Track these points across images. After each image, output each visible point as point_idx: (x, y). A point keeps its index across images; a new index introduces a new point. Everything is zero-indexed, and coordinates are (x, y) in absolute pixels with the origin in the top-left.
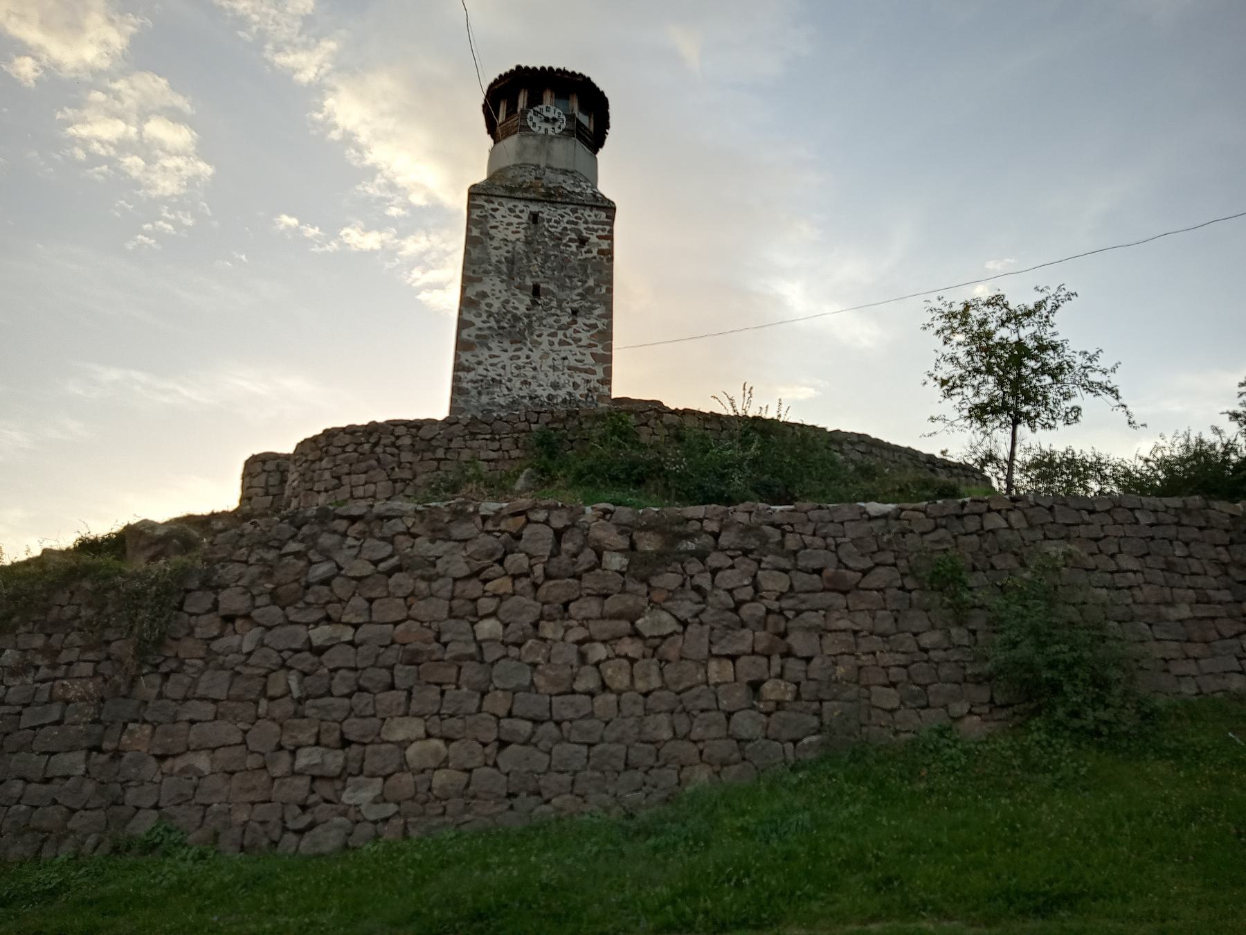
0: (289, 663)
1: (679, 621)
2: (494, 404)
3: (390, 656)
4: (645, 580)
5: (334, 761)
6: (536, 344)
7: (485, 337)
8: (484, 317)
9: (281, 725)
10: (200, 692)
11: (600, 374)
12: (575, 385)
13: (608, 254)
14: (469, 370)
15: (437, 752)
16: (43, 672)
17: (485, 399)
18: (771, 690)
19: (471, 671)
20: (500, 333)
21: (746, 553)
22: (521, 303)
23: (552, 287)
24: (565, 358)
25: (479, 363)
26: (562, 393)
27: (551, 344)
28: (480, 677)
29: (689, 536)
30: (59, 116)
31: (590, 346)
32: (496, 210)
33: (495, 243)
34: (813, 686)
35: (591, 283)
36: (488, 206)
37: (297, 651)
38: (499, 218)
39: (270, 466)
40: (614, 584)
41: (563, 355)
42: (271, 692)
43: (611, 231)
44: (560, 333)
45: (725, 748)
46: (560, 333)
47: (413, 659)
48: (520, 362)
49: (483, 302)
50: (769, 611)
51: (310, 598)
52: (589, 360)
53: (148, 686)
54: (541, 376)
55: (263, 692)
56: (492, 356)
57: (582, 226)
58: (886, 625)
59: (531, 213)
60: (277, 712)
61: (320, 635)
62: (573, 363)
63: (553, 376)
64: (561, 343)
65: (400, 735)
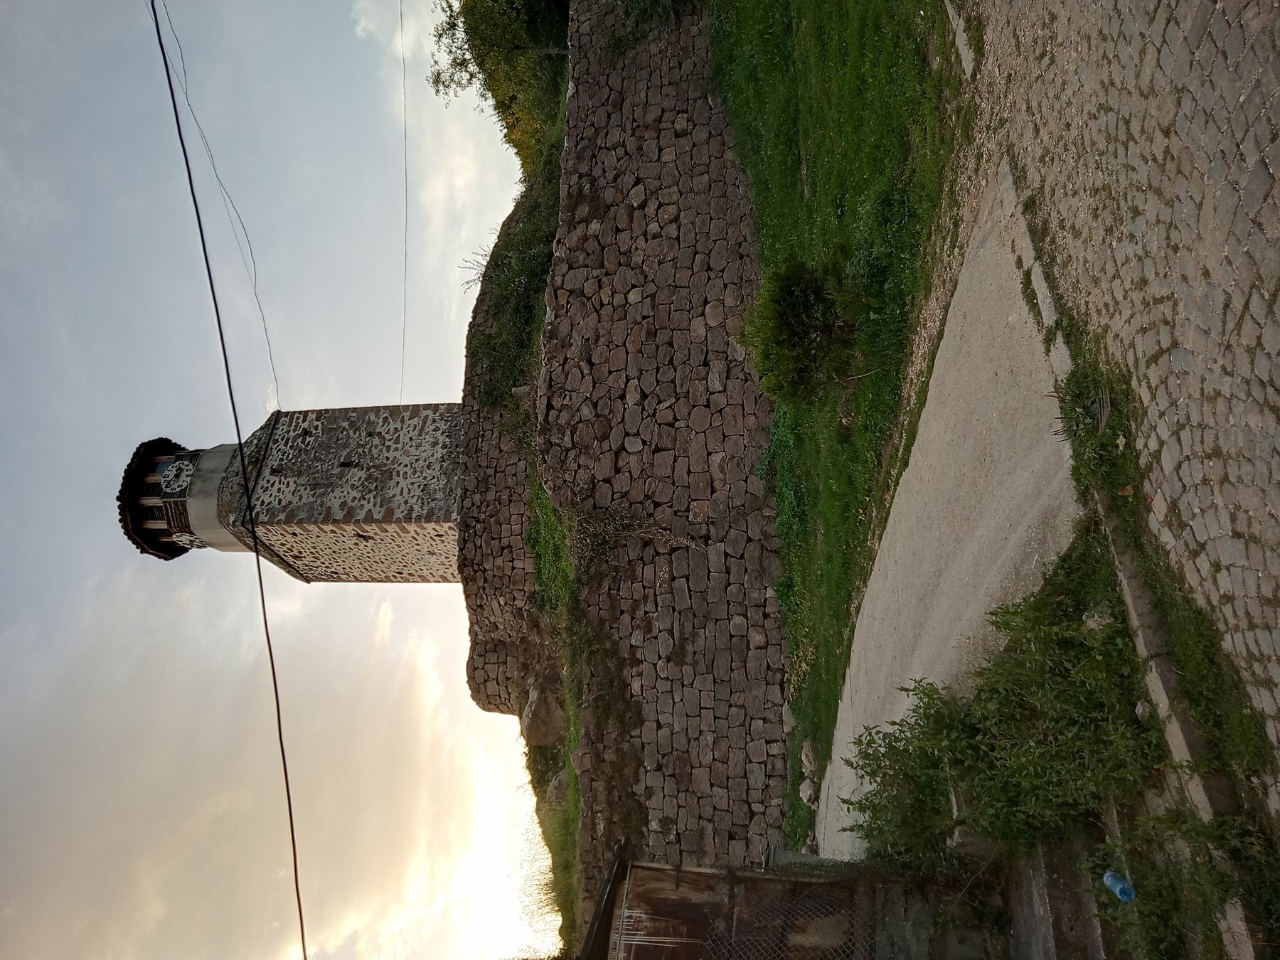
0: (651, 412)
1: (636, 184)
2: (444, 488)
3: (649, 349)
4: (608, 207)
5: (717, 366)
8: (364, 502)
10: (668, 473)
11: (430, 413)
12: (436, 429)
13: (320, 414)
14: (412, 509)
15: (714, 307)
16: (650, 606)
17: (439, 495)
18: (681, 123)
19: (661, 298)
20: (381, 487)
21: (594, 156)
22: (356, 475)
23: (345, 453)
25: (406, 502)
26: (441, 439)
27: (397, 449)
29: (581, 189)
31: (402, 421)
32: (263, 502)
34: (679, 103)
35: (345, 424)
36: (258, 508)
37: (643, 409)
38: (272, 499)
39: (479, 663)
43: (300, 413)
44: (387, 443)
45: (715, 143)
46: (387, 443)
47: (652, 334)
48: (410, 472)
49: (350, 504)
50: (633, 135)
51: (607, 412)
52: (415, 421)
54: (424, 455)
55: (672, 425)
57: (292, 434)
58: (644, 73)
59: (271, 474)
60: (685, 411)
61: (632, 398)
62: (416, 432)
63: (426, 446)
64: (397, 442)
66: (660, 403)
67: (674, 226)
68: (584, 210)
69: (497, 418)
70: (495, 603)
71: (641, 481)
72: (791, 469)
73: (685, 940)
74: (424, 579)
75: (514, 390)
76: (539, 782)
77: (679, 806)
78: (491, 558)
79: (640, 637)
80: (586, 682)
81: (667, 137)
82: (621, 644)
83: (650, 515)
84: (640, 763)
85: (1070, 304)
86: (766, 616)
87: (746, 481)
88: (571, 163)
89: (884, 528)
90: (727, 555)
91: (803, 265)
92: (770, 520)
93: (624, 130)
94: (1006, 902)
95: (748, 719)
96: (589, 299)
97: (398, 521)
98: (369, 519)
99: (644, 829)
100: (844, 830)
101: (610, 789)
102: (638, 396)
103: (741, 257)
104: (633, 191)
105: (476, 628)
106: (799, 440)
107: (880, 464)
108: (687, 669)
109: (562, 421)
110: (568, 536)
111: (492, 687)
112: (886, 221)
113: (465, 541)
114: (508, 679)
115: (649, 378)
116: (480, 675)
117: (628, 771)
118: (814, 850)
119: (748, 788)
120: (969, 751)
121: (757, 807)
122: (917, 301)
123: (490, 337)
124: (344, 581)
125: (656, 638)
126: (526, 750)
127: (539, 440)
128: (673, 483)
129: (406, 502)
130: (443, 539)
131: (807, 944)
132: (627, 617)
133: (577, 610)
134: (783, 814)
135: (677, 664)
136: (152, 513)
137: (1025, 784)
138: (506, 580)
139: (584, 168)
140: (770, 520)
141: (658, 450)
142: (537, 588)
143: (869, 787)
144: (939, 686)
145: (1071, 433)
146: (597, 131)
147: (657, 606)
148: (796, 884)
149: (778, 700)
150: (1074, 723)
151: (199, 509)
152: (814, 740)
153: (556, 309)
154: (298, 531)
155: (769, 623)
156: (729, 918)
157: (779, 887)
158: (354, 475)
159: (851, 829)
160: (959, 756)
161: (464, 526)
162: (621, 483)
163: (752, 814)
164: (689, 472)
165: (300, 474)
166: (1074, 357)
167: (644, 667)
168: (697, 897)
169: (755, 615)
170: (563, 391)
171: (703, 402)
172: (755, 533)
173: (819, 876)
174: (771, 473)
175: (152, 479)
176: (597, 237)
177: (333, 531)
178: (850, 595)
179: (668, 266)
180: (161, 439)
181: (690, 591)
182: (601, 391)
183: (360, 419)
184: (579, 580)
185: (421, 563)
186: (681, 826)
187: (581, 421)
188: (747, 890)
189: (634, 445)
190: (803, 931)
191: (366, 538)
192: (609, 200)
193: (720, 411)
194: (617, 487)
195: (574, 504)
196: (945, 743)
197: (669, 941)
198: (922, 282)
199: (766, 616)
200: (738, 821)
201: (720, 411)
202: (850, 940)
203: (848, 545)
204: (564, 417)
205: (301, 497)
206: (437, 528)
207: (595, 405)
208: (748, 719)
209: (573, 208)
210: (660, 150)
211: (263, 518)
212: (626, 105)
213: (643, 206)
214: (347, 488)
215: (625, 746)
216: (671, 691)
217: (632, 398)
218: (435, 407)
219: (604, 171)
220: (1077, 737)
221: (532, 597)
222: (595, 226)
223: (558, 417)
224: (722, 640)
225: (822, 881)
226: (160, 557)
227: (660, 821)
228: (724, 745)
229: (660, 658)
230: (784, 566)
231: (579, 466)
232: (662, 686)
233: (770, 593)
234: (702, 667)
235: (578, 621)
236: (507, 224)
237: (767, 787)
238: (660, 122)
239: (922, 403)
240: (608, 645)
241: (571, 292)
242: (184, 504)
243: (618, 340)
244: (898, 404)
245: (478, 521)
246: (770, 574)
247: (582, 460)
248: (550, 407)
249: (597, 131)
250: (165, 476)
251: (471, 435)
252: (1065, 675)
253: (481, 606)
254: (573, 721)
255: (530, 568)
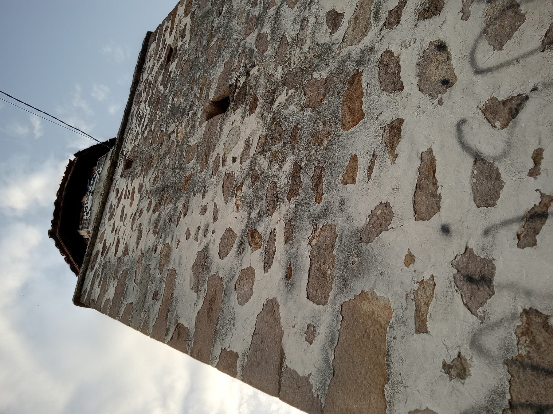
7: (321, 253)
8: (254, 258)
30: (21, 130)
56: (427, 194)
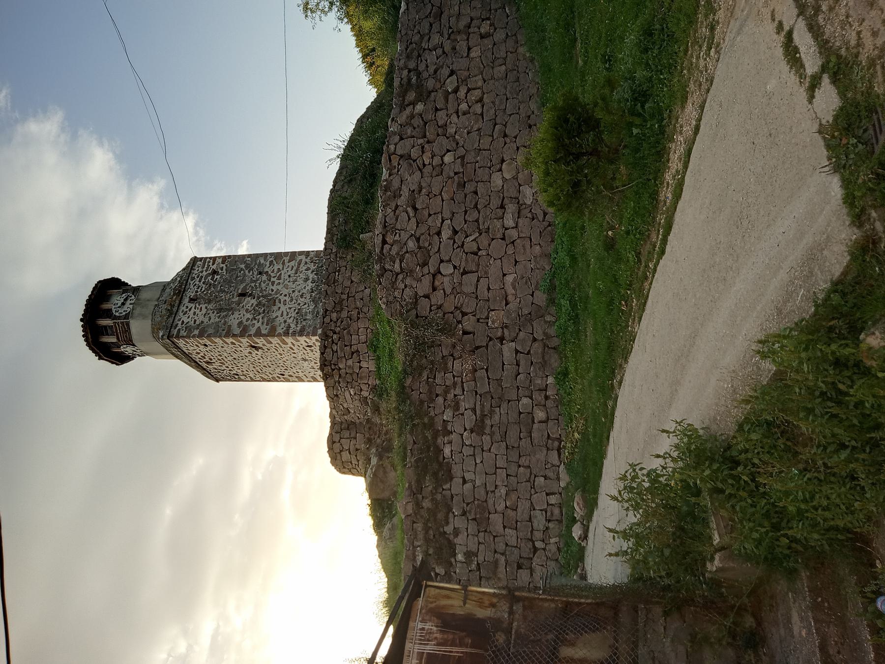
2: (313, 312)
3: (459, 197)
4: (430, 92)
5: (511, 208)
6: (278, 292)
8: (255, 322)
9: (493, 239)
10: (473, 289)
11: (303, 257)
13: (224, 259)
14: (289, 327)
15: (510, 164)
16: (458, 391)
17: (309, 317)
18: (485, 28)
19: (469, 158)
21: (419, 56)
22: (249, 302)
23: (242, 286)
24: (289, 276)
25: (285, 322)
26: (311, 276)
28: (473, 153)
29: (409, 80)
31: (283, 263)
33: (206, 320)
35: (243, 266)
36: (179, 326)
37: (454, 242)
38: (189, 320)
40: (430, 106)
41: (287, 277)
42: (475, 249)
43: (210, 258)
44: (272, 279)
45: (510, 43)
46: (272, 279)
49: (245, 323)
50: (449, 39)
51: (426, 245)
52: (292, 263)
53: (468, 323)
54: (299, 287)
55: (476, 254)
56: (282, 315)
57: (205, 273)
60: (486, 243)
61: (446, 234)
62: (293, 272)
64: (279, 278)
65: (500, 182)
66: (467, 236)
67: (479, 105)
68: (411, 96)
69: (349, 257)
70: (347, 394)
71: (452, 297)
72: (567, 283)
73: (468, 650)
74: (300, 380)
75: (361, 236)
76: (378, 526)
77: (479, 543)
78: (344, 360)
79: (451, 414)
80: (409, 448)
81: (474, 39)
82: (436, 419)
83: (459, 322)
84: (450, 510)
85: (838, 44)
86: (547, 398)
87: (532, 295)
88: (402, 62)
89: (643, 310)
90: (517, 352)
91: (576, 99)
92: (551, 324)
93: (442, 35)
94: (759, 623)
95: (533, 476)
96: (414, 161)
97: (279, 335)
98: (258, 334)
99: (453, 560)
100: (610, 555)
101: (426, 529)
102: (450, 232)
103: (530, 127)
104: (448, 80)
105: (334, 412)
106: (573, 259)
107: (640, 261)
108: (486, 439)
109: (393, 252)
110: (397, 340)
111: (345, 456)
112: (646, 50)
113: (325, 347)
114: (357, 450)
115: (459, 218)
116: (337, 446)
117: (440, 516)
118: (583, 577)
119: (533, 529)
120: (730, 481)
121: (539, 544)
122: (674, 113)
123: (345, 198)
124: (243, 381)
125: (462, 414)
126: (369, 502)
127: (377, 267)
128: (477, 298)
129: (285, 322)
130: (309, 348)
131: (576, 656)
132: (440, 400)
133: (403, 394)
134: (559, 549)
135: (478, 434)
136: (105, 331)
137: (792, 509)
138: (355, 376)
139: (412, 65)
140: (551, 324)
141: (465, 273)
142: (378, 382)
143: (633, 518)
144: (697, 425)
145: (837, 168)
146: (422, 37)
147: (463, 390)
148: (567, 604)
149: (557, 462)
150: (843, 446)
151: (139, 327)
152: (584, 491)
153: (390, 170)
154: (208, 343)
155: (549, 403)
156: (508, 631)
157: (553, 605)
158: (248, 302)
159: (617, 555)
160: (720, 485)
161: (325, 337)
162: (437, 298)
163: (535, 550)
164: (489, 289)
165: (209, 302)
166: (842, 94)
167: (453, 437)
168: (482, 613)
169: (538, 397)
170: (394, 230)
171: (499, 235)
172: (539, 335)
173: (587, 597)
174: (551, 289)
175: (105, 306)
176: (421, 115)
177: (233, 343)
178: (613, 372)
179: (474, 134)
180: (113, 278)
181: (489, 378)
182: (423, 229)
183: (253, 262)
184: (405, 371)
185: (298, 367)
186: (481, 558)
187: (407, 252)
188: (524, 607)
189: (447, 269)
190: (572, 644)
191: (257, 348)
192: (430, 87)
193: (513, 242)
194: (434, 301)
195: (401, 314)
196: (707, 472)
197: (456, 651)
198: (679, 95)
199: (547, 398)
200: (524, 555)
201: (513, 242)
202: (615, 654)
203: (612, 332)
204: (395, 249)
205: (210, 318)
206: (308, 340)
207: (418, 240)
208: (533, 476)
209: (403, 94)
210: (469, 49)
211: (183, 333)
212: (444, 16)
213: (456, 91)
214: (243, 312)
215: (439, 497)
216: (474, 455)
217: (446, 234)
218: (307, 254)
219: (427, 66)
220: (848, 461)
221: (374, 389)
222: (420, 107)
223: (390, 249)
224: (513, 417)
225: (589, 601)
226: (113, 363)
227: (465, 554)
228: (514, 496)
229: (465, 430)
230: (561, 359)
231: (406, 286)
232: (467, 451)
233: (550, 380)
234: (497, 437)
235: (404, 401)
236: (360, 121)
237: (547, 528)
238: (469, 27)
239: (678, 196)
240: (426, 420)
241: (401, 156)
242: (128, 324)
243: (436, 190)
244: (656, 207)
245: (335, 333)
246: (550, 365)
247: (408, 281)
248: (384, 242)
249: (422, 37)
250: (116, 303)
251: (331, 270)
252: (839, 398)
253: (337, 395)
254: (400, 478)
255: (373, 368)
